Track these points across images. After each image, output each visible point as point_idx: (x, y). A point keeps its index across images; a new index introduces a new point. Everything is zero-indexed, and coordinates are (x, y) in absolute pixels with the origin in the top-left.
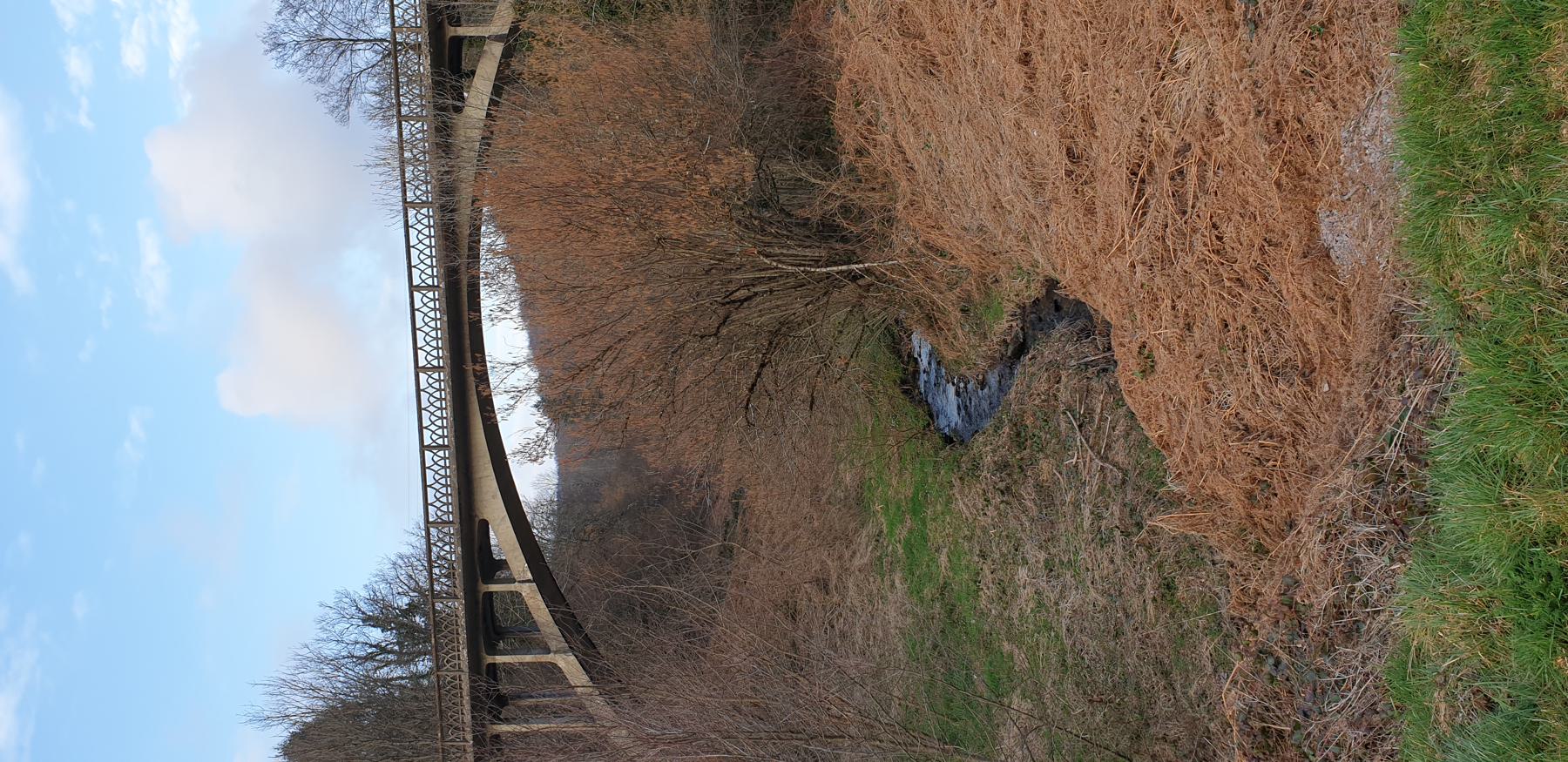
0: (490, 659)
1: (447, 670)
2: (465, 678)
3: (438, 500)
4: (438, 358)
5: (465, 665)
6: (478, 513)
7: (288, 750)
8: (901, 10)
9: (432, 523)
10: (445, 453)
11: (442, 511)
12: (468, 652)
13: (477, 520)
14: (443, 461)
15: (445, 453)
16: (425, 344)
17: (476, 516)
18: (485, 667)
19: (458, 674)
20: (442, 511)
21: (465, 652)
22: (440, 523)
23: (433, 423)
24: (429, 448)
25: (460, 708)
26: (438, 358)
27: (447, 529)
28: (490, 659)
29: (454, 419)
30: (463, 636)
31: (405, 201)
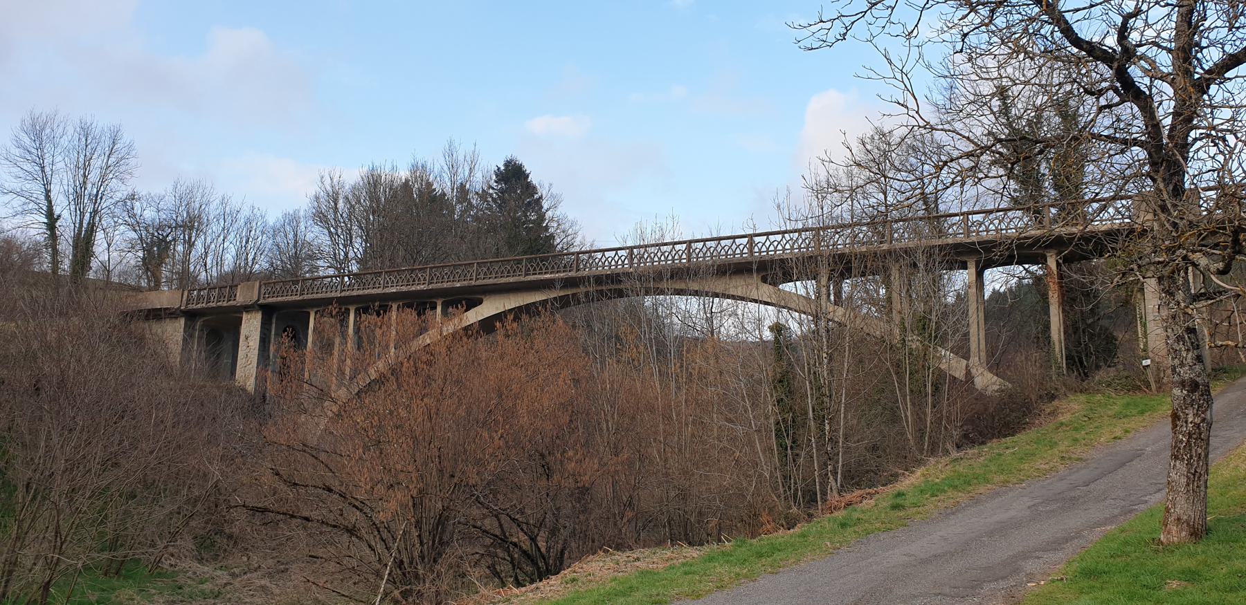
0: (395, 306)
1: (385, 278)
2: (379, 291)
3: (607, 259)
4: (760, 252)
5: (387, 290)
6: (487, 297)
7: (9, 245)
8: (163, 507)
9: (752, 239)
10: (738, 254)
11: (675, 255)
12: (393, 292)
13: (483, 297)
14: (765, 250)
15: (738, 254)
16: (620, 256)
17: (486, 296)
18: (308, 310)
19: (382, 286)
20: (675, 255)
21: (394, 291)
22: (751, 244)
23: (723, 248)
24: (631, 253)
25: (411, 283)
26: (760, 252)
27: (685, 257)
28: (395, 306)
29: (541, 280)
30: (404, 289)
31: (691, 242)
